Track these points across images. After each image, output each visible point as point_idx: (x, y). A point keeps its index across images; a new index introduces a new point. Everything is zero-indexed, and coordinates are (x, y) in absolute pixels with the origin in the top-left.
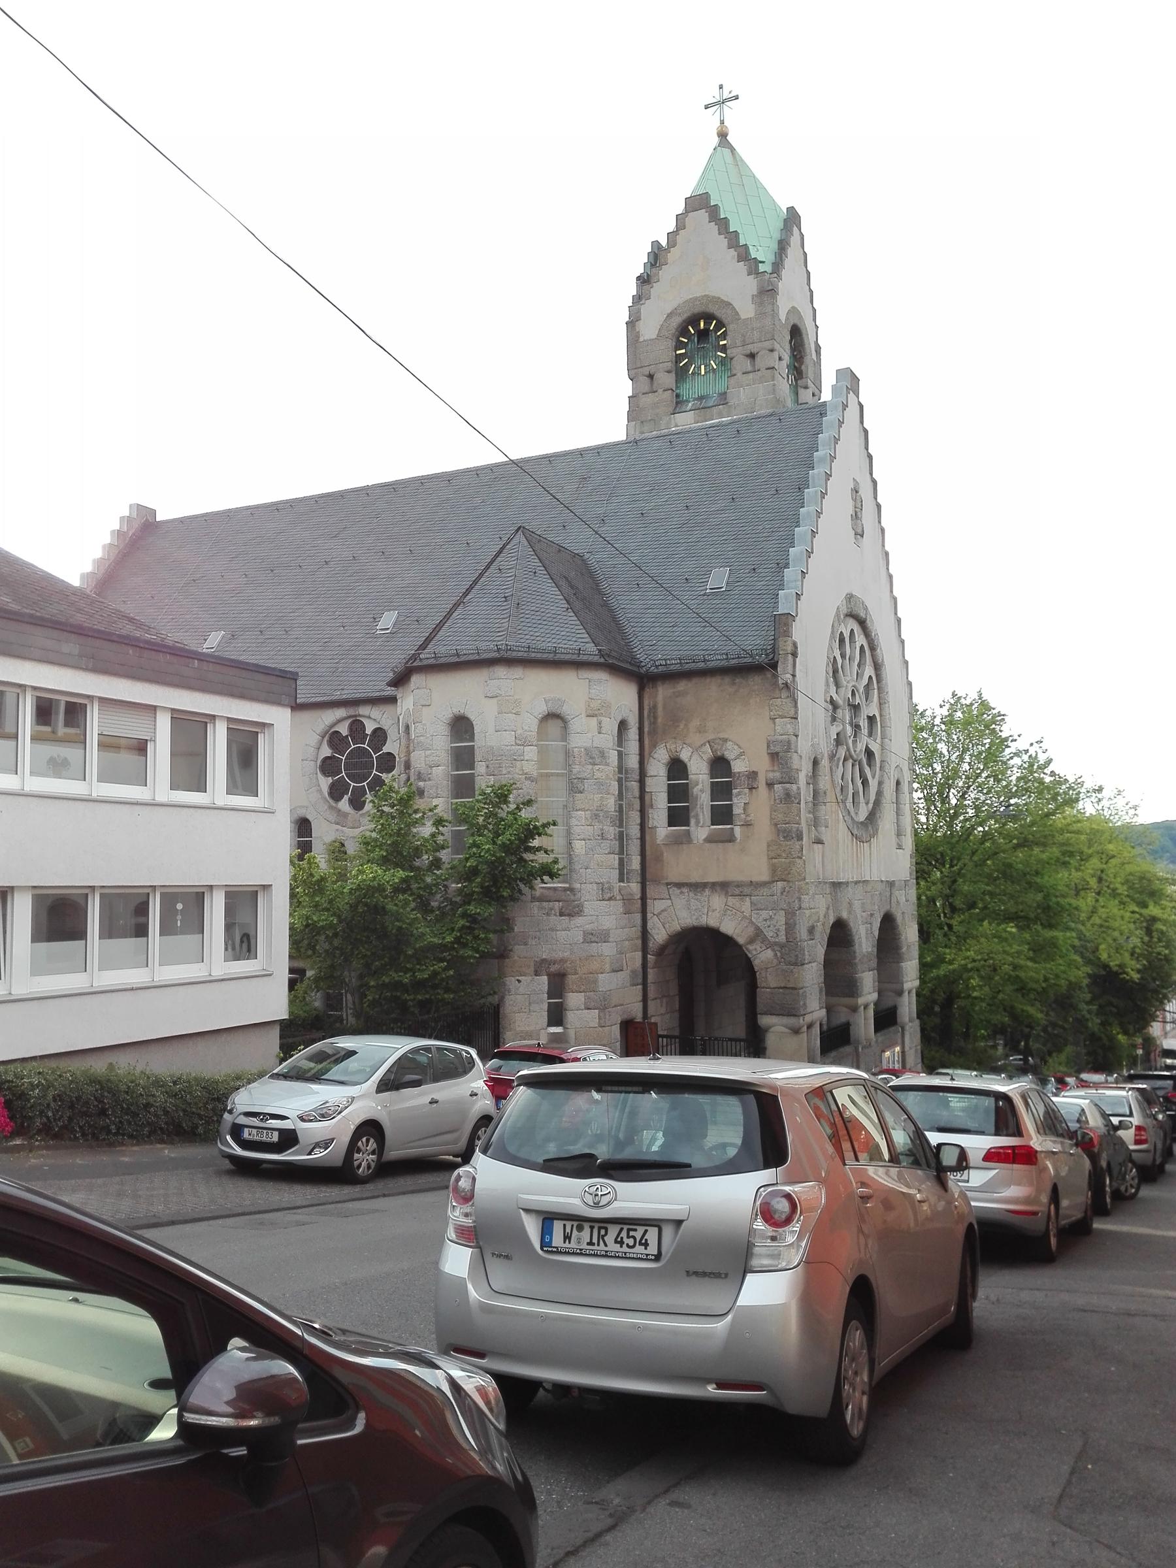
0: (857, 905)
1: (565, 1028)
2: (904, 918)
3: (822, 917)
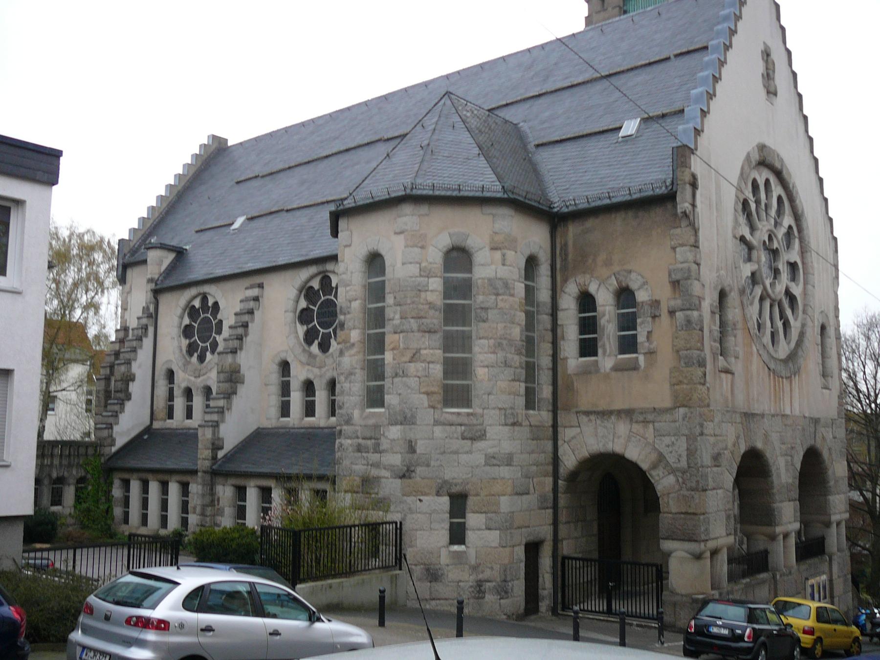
0: (774, 437)
1: (467, 547)
2: (830, 454)
3: (730, 445)
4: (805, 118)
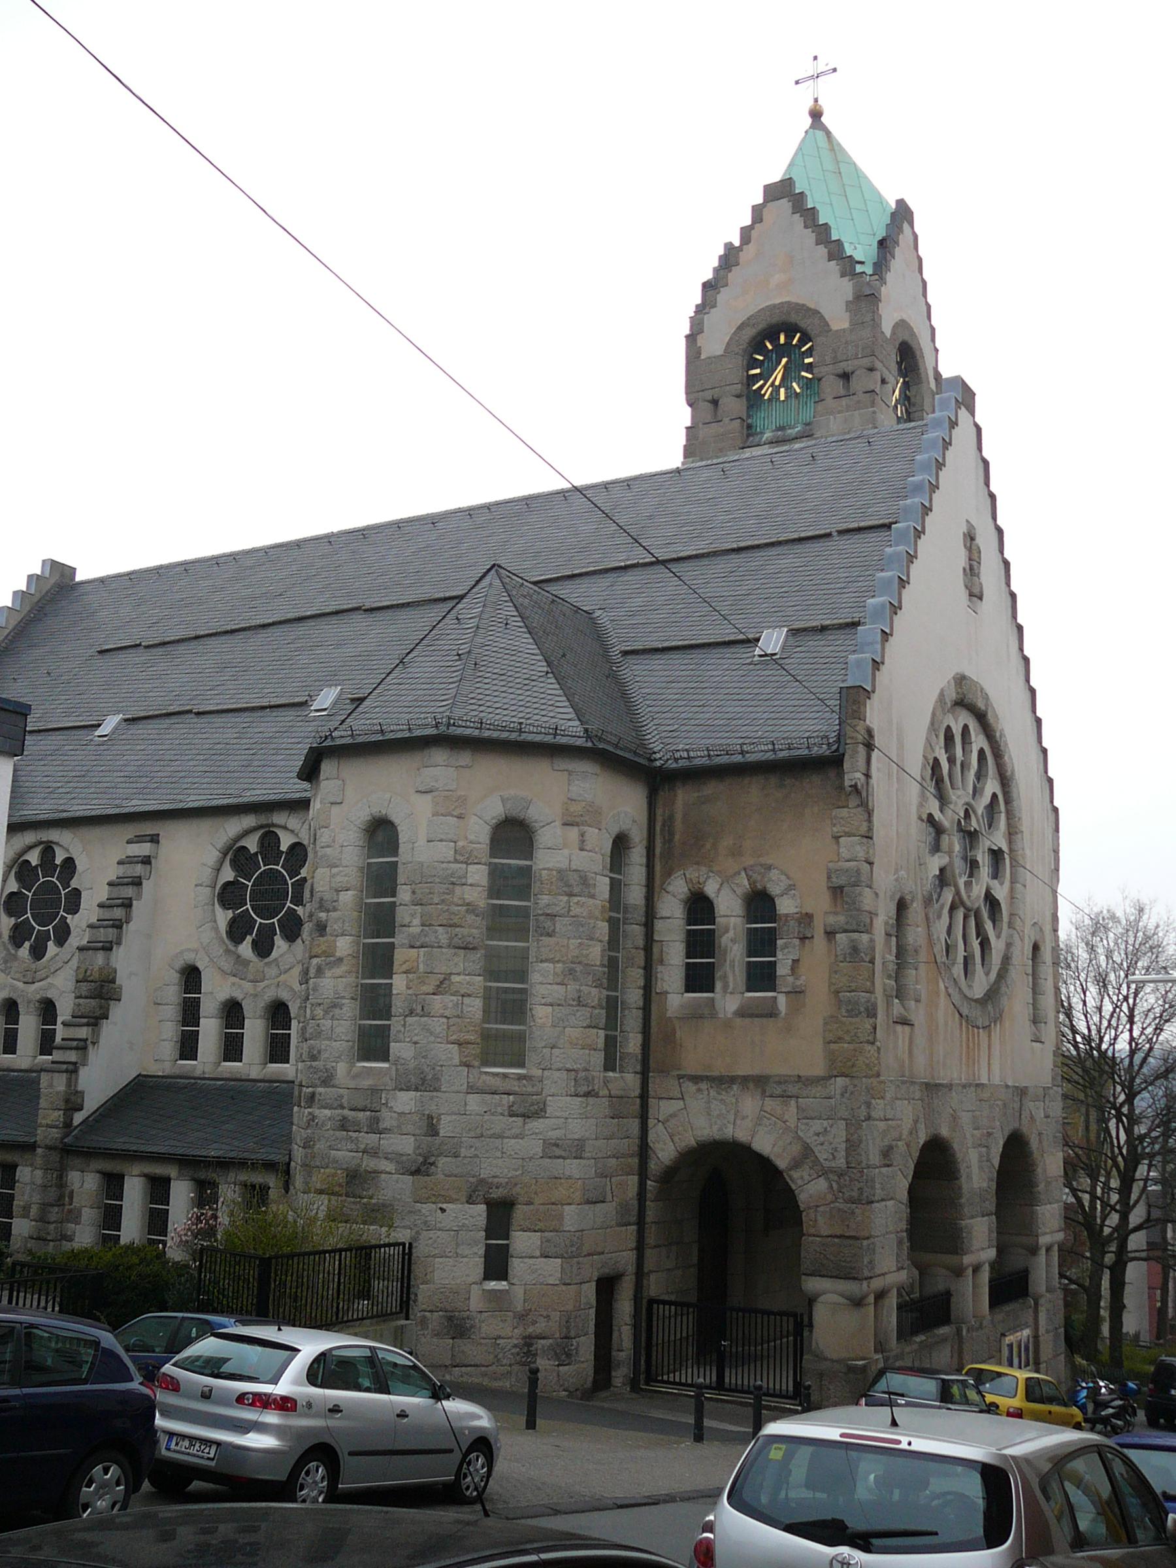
0: (965, 1118)
2: (1040, 1142)
3: (905, 1133)
4: (1020, 628)
